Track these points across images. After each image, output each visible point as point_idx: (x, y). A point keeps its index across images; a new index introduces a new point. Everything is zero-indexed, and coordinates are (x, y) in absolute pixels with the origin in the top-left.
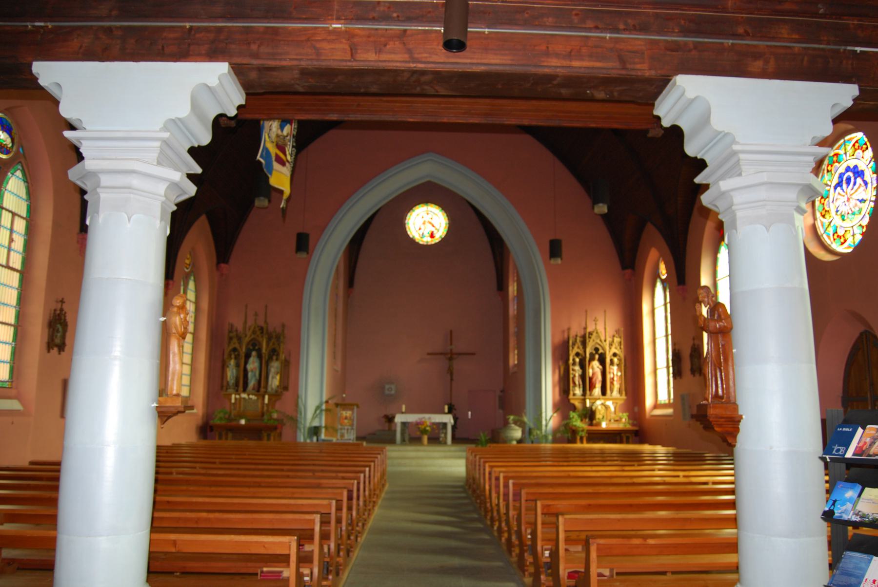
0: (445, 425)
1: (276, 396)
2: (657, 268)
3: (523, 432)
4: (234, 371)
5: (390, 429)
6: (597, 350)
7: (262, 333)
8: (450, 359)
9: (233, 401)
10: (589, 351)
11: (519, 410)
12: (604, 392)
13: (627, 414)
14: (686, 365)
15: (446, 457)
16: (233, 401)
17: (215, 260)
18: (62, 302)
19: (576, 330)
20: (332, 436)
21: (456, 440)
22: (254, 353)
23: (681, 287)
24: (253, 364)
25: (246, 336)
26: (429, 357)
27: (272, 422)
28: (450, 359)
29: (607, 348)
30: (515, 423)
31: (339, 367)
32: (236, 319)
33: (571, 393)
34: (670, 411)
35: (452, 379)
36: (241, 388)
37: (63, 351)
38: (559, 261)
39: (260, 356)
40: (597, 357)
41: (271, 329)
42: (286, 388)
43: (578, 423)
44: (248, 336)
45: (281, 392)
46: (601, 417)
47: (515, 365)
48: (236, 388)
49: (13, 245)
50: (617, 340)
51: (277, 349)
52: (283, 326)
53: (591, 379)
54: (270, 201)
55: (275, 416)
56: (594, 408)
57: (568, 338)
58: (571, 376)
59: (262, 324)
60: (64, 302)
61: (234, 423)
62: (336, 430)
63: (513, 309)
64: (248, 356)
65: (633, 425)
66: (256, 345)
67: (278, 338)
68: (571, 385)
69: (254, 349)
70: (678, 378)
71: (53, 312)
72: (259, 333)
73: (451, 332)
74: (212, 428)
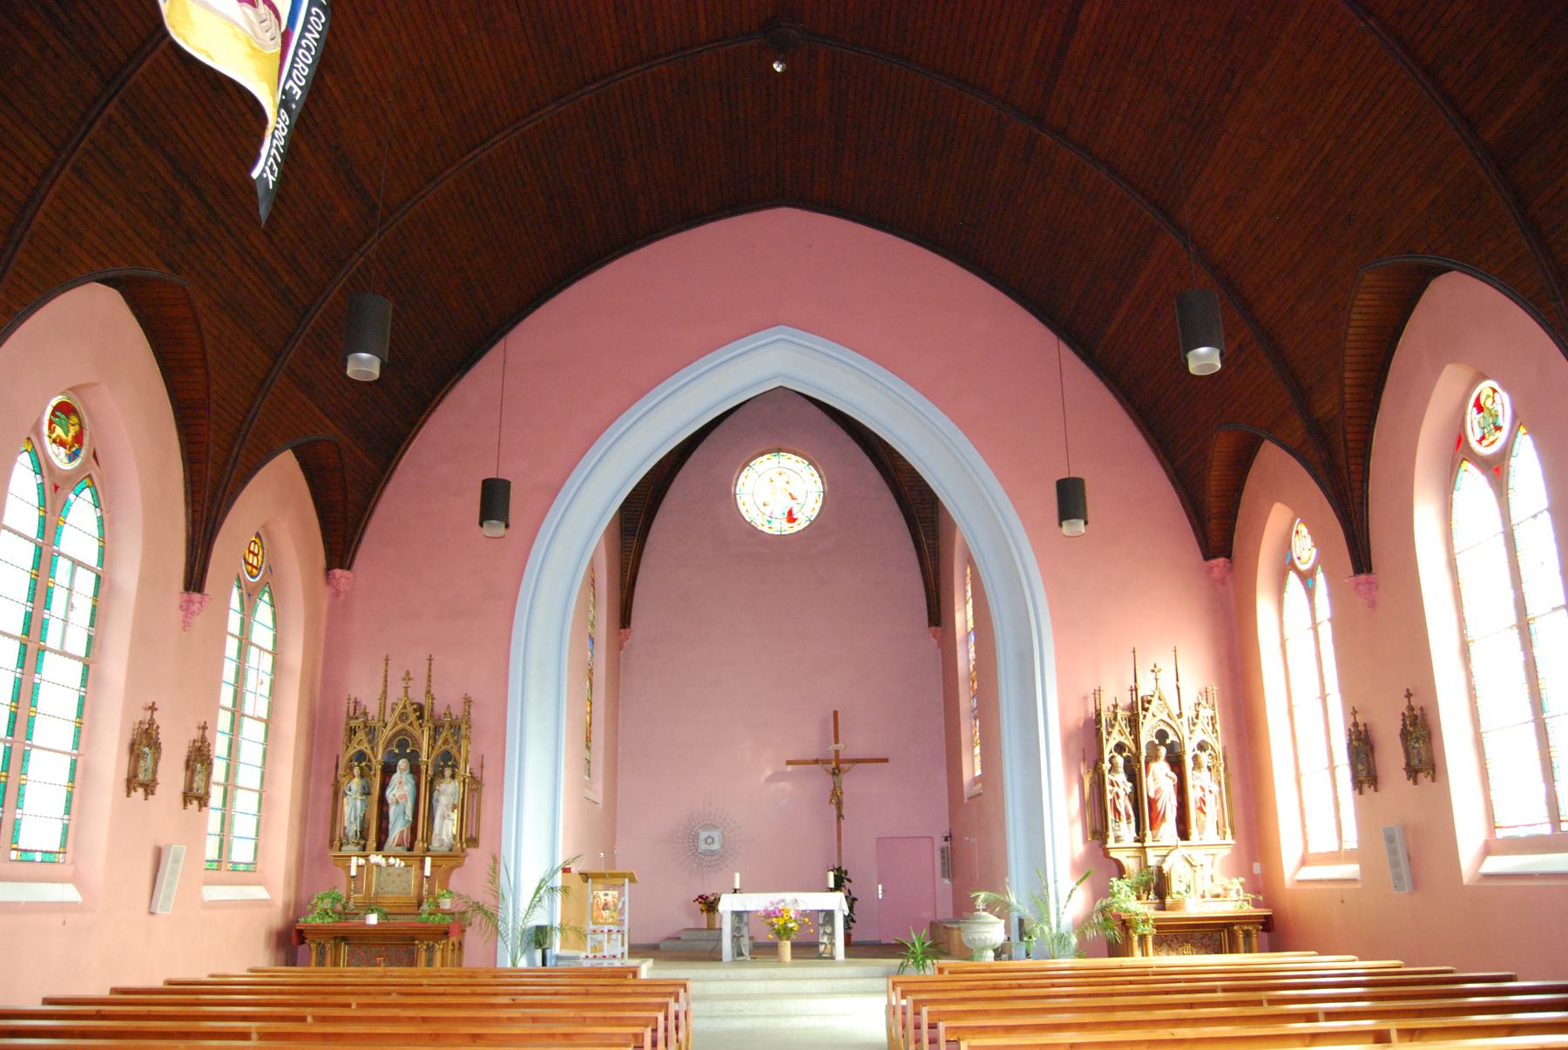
0: (829, 915)
1: (452, 858)
2: (1287, 545)
3: (1007, 929)
4: (359, 803)
5: (711, 927)
6: (1162, 735)
7: (421, 717)
8: (836, 772)
9: (353, 872)
10: (1147, 735)
11: (994, 879)
12: (1184, 833)
13: (1242, 879)
14: (1391, 756)
15: (833, 993)
16: (353, 872)
17: (321, 561)
18: (153, 708)
19: (1115, 694)
20: (579, 949)
21: (855, 948)
22: (403, 764)
23: (1362, 577)
24: (401, 788)
25: (385, 725)
26: (790, 768)
27: (438, 918)
28: (836, 772)
29: (1185, 731)
30: (989, 907)
31: (598, 794)
32: (364, 689)
33: (1111, 834)
34: (1351, 870)
35: (840, 816)
36: (372, 842)
37: (153, 794)
38: (1078, 527)
39: (415, 770)
40: (1163, 751)
41: (440, 709)
42: (473, 841)
43: (1141, 908)
44: (390, 726)
45: (463, 850)
46: (1182, 888)
47: (976, 781)
48: (362, 842)
49: (72, 615)
50: (1206, 713)
51: (454, 752)
52: (468, 701)
53: (1152, 802)
54: (507, 526)
55: (446, 904)
56: (1166, 868)
57: (1098, 715)
58: (1109, 797)
59: (420, 697)
60: (156, 709)
61: (354, 922)
62: (581, 935)
63: (966, 656)
64: (388, 770)
65: (1256, 904)
66: (408, 746)
67: (456, 727)
68: (1111, 816)
69: (402, 755)
70: (1368, 790)
71: (192, 744)
72: (412, 717)
73: (836, 713)
74: (301, 936)
